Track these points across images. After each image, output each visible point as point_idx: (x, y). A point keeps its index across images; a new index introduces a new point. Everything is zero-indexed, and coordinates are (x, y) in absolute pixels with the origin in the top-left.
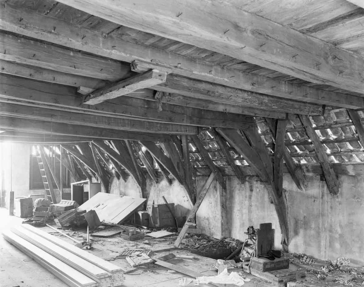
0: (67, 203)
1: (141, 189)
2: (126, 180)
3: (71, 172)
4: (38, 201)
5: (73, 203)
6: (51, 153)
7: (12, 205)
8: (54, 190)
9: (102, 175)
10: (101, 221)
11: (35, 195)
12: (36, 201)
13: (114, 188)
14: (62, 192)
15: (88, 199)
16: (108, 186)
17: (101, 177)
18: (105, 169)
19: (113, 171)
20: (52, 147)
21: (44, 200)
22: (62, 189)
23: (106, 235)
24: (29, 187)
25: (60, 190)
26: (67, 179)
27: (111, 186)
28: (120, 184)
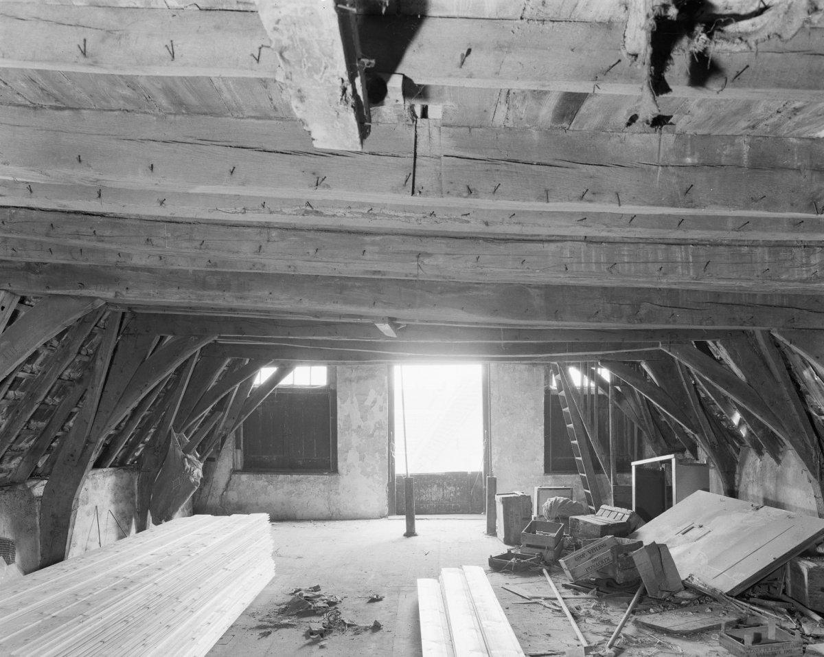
0: (613, 515)
1: (818, 488)
2: (780, 457)
3: (644, 432)
4: (551, 504)
5: (628, 516)
6: (593, 385)
7: (492, 511)
8: (597, 476)
9: (715, 441)
10: (683, 576)
11: (551, 489)
12: (546, 504)
13: (747, 480)
14: (615, 483)
15: (670, 506)
16: (734, 472)
17: (712, 447)
18: (724, 424)
19: (743, 432)
20: (594, 369)
21: (564, 502)
22: (613, 475)
23: (676, 629)
24: (543, 468)
25: (610, 477)
26: (636, 448)
27: (740, 475)
28: (763, 467)
